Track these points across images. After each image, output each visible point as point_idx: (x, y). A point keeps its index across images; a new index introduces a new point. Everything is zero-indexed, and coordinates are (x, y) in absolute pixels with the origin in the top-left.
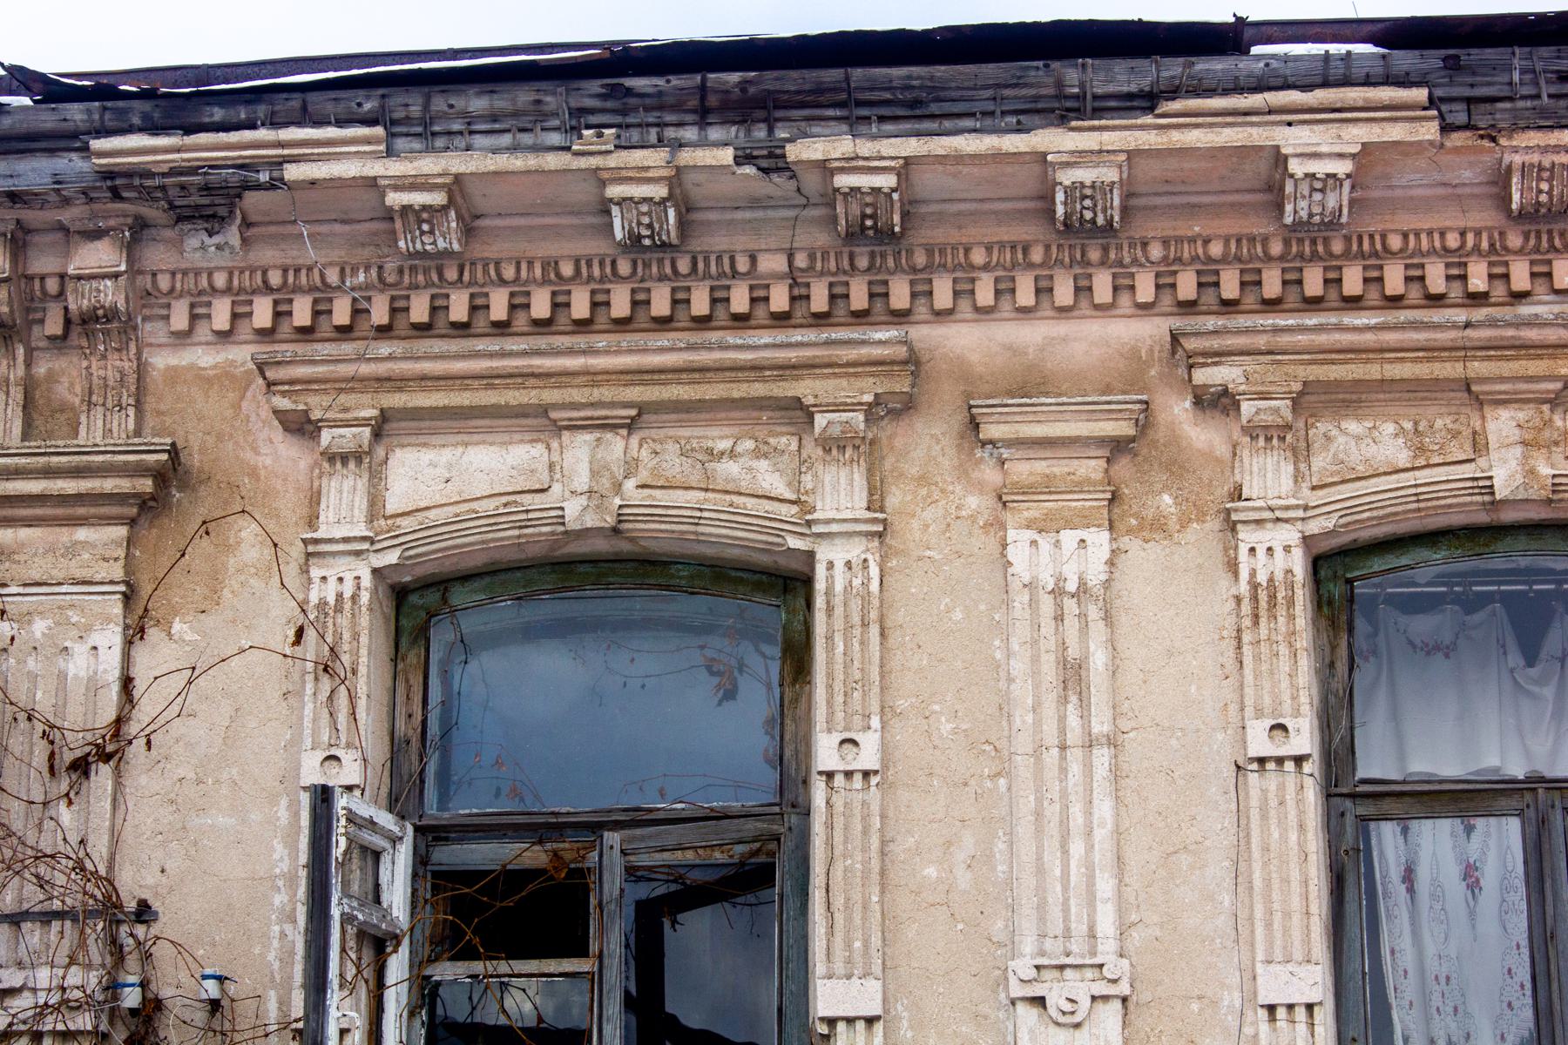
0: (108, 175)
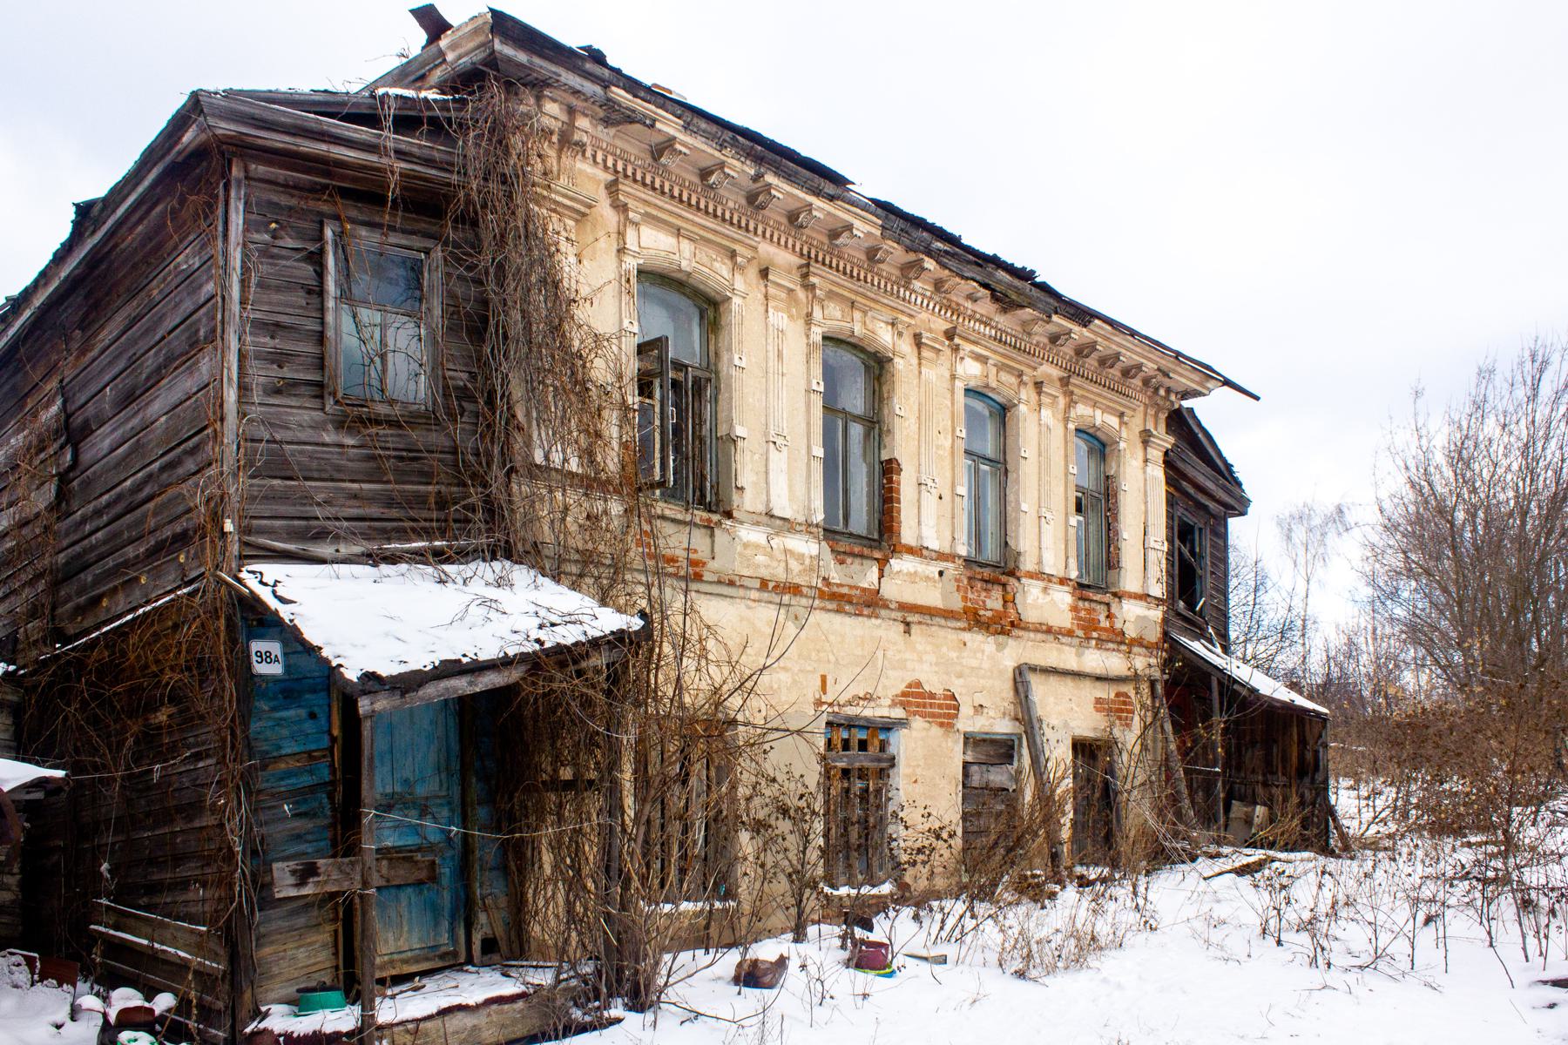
0: (609, 100)
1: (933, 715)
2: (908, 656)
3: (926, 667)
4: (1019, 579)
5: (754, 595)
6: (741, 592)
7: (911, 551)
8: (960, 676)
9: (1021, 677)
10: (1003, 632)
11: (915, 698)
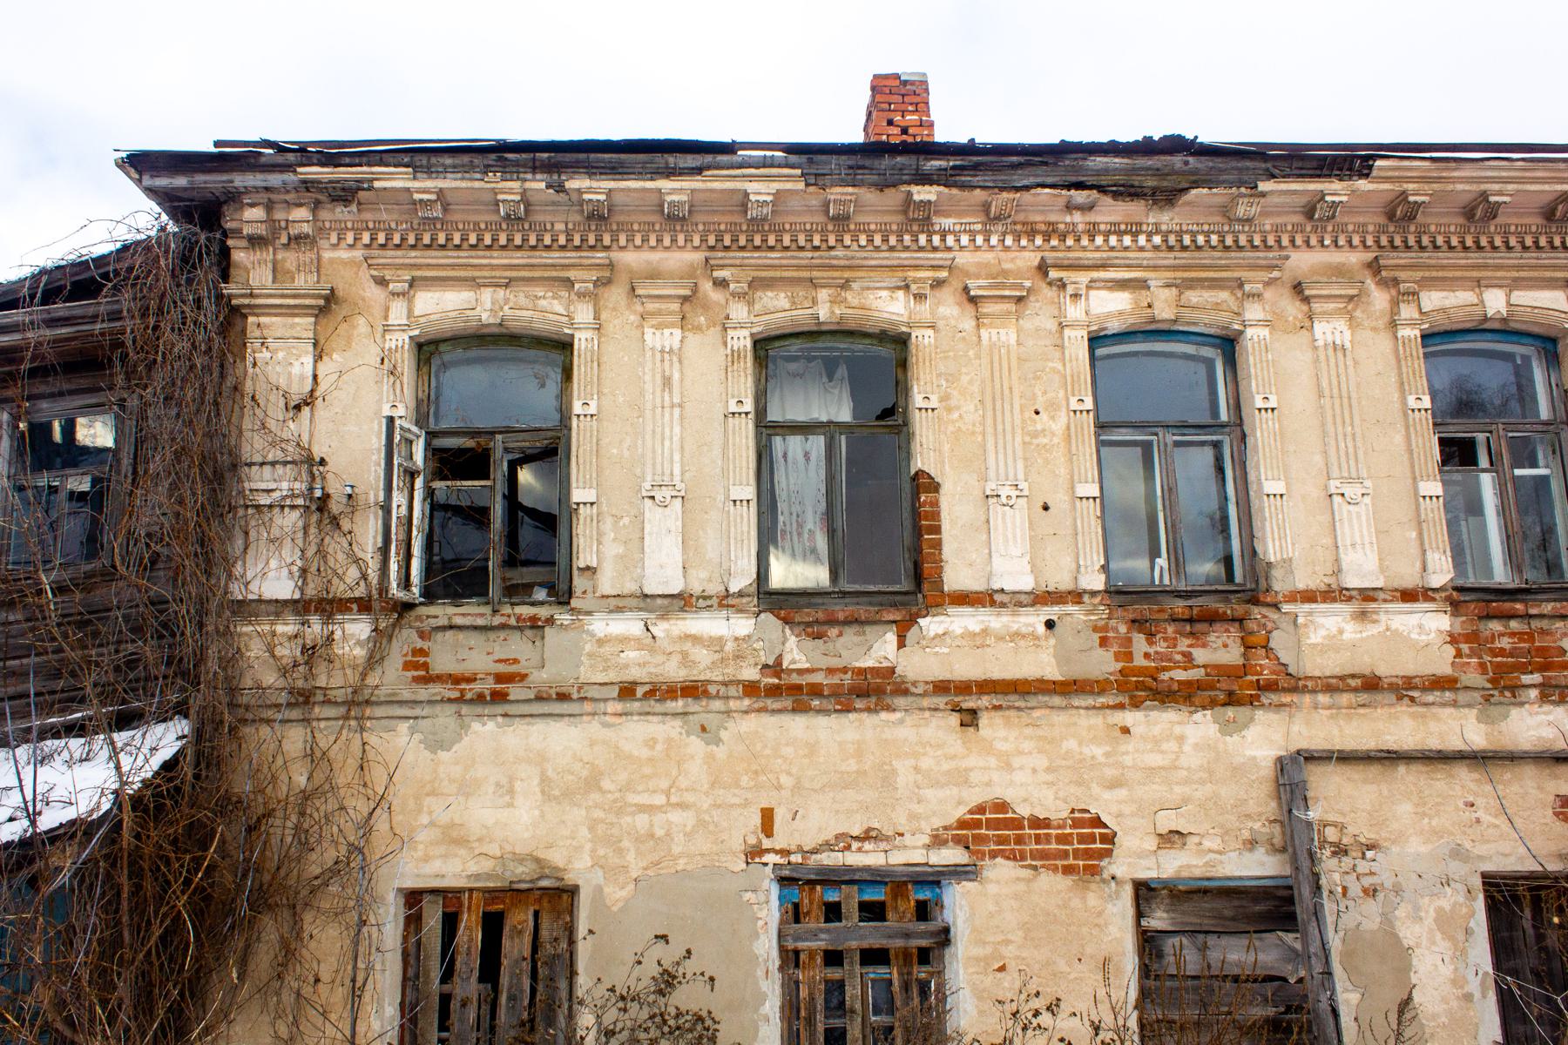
1: (1044, 855)
2: (972, 761)
3: (1019, 777)
4: (1276, 606)
5: (613, 707)
6: (588, 707)
7: (964, 599)
8: (1114, 784)
9: (1291, 778)
10: (1232, 700)
11: (992, 831)
